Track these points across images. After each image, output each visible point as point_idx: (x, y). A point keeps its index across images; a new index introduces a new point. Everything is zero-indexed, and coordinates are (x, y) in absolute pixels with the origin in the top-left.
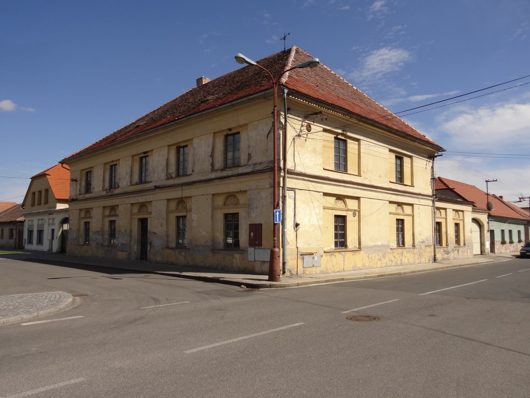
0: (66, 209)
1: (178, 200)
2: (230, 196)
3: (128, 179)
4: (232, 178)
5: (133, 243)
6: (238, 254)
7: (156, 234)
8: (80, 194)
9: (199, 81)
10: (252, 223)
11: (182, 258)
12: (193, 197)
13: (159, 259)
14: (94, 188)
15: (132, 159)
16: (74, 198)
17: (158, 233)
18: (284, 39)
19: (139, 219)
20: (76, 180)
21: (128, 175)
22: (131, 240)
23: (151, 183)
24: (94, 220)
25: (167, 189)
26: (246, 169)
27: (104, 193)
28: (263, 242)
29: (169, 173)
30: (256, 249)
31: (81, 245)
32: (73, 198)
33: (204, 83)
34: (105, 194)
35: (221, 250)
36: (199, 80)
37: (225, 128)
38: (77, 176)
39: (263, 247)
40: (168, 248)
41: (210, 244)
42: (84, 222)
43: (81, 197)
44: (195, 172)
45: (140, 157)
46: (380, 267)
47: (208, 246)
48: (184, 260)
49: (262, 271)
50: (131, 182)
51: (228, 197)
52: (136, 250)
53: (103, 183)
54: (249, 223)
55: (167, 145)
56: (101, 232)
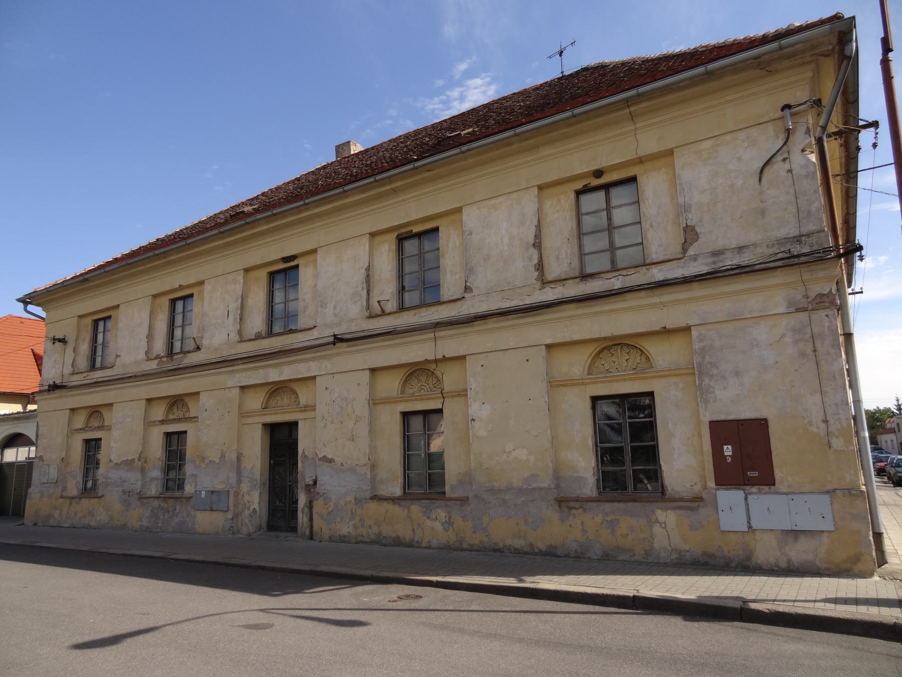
0: (18, 413)
2: (608, 348)
3: (231, 325)
4: (628, 296)
5: (245, 487)
6: (669, 512)
7: (331, 461)
8: (73, 374)
9: (343, 149)
10: (716, 418)
11: (438, 526)
12: (472, 357)
13: (345, 528)
14: (119, 356)
15: (245, 278)
16: (58, 382)
17: (338, 460)
18: (560, 55)
19: (265, 425)
20: (64, 339)
21: (231, 318)
22: (239, 481)
23: (312, 331)
24: (116, 433)
25: (377, 342)
26: (682, 267)
27: (153, 365)
28: (778, 474)
29: (379, 302)
30: (750, 493)
31: (73, 498)
32: (54, 382)
33: (352, 153)
34: (155, 367)
35: (590, 500)
36: (340, 148)
37: (586, 170)
38: (67, 329)
39: (780, 486)
40: (376, 498)
41: (546, 482)
42: (84, 440)
43: (77, 380)
44: (475, 292)
45: (268, 272)
46: (368, 495)
47: (541, 489)
48: (446, 530)
49: (789, 561)
50: (240, 332)
51: (92, 414)
52: (256, 506)
53: (148, 342)
54: (706, 417)
55: (369, 231)
56: (140, 463)
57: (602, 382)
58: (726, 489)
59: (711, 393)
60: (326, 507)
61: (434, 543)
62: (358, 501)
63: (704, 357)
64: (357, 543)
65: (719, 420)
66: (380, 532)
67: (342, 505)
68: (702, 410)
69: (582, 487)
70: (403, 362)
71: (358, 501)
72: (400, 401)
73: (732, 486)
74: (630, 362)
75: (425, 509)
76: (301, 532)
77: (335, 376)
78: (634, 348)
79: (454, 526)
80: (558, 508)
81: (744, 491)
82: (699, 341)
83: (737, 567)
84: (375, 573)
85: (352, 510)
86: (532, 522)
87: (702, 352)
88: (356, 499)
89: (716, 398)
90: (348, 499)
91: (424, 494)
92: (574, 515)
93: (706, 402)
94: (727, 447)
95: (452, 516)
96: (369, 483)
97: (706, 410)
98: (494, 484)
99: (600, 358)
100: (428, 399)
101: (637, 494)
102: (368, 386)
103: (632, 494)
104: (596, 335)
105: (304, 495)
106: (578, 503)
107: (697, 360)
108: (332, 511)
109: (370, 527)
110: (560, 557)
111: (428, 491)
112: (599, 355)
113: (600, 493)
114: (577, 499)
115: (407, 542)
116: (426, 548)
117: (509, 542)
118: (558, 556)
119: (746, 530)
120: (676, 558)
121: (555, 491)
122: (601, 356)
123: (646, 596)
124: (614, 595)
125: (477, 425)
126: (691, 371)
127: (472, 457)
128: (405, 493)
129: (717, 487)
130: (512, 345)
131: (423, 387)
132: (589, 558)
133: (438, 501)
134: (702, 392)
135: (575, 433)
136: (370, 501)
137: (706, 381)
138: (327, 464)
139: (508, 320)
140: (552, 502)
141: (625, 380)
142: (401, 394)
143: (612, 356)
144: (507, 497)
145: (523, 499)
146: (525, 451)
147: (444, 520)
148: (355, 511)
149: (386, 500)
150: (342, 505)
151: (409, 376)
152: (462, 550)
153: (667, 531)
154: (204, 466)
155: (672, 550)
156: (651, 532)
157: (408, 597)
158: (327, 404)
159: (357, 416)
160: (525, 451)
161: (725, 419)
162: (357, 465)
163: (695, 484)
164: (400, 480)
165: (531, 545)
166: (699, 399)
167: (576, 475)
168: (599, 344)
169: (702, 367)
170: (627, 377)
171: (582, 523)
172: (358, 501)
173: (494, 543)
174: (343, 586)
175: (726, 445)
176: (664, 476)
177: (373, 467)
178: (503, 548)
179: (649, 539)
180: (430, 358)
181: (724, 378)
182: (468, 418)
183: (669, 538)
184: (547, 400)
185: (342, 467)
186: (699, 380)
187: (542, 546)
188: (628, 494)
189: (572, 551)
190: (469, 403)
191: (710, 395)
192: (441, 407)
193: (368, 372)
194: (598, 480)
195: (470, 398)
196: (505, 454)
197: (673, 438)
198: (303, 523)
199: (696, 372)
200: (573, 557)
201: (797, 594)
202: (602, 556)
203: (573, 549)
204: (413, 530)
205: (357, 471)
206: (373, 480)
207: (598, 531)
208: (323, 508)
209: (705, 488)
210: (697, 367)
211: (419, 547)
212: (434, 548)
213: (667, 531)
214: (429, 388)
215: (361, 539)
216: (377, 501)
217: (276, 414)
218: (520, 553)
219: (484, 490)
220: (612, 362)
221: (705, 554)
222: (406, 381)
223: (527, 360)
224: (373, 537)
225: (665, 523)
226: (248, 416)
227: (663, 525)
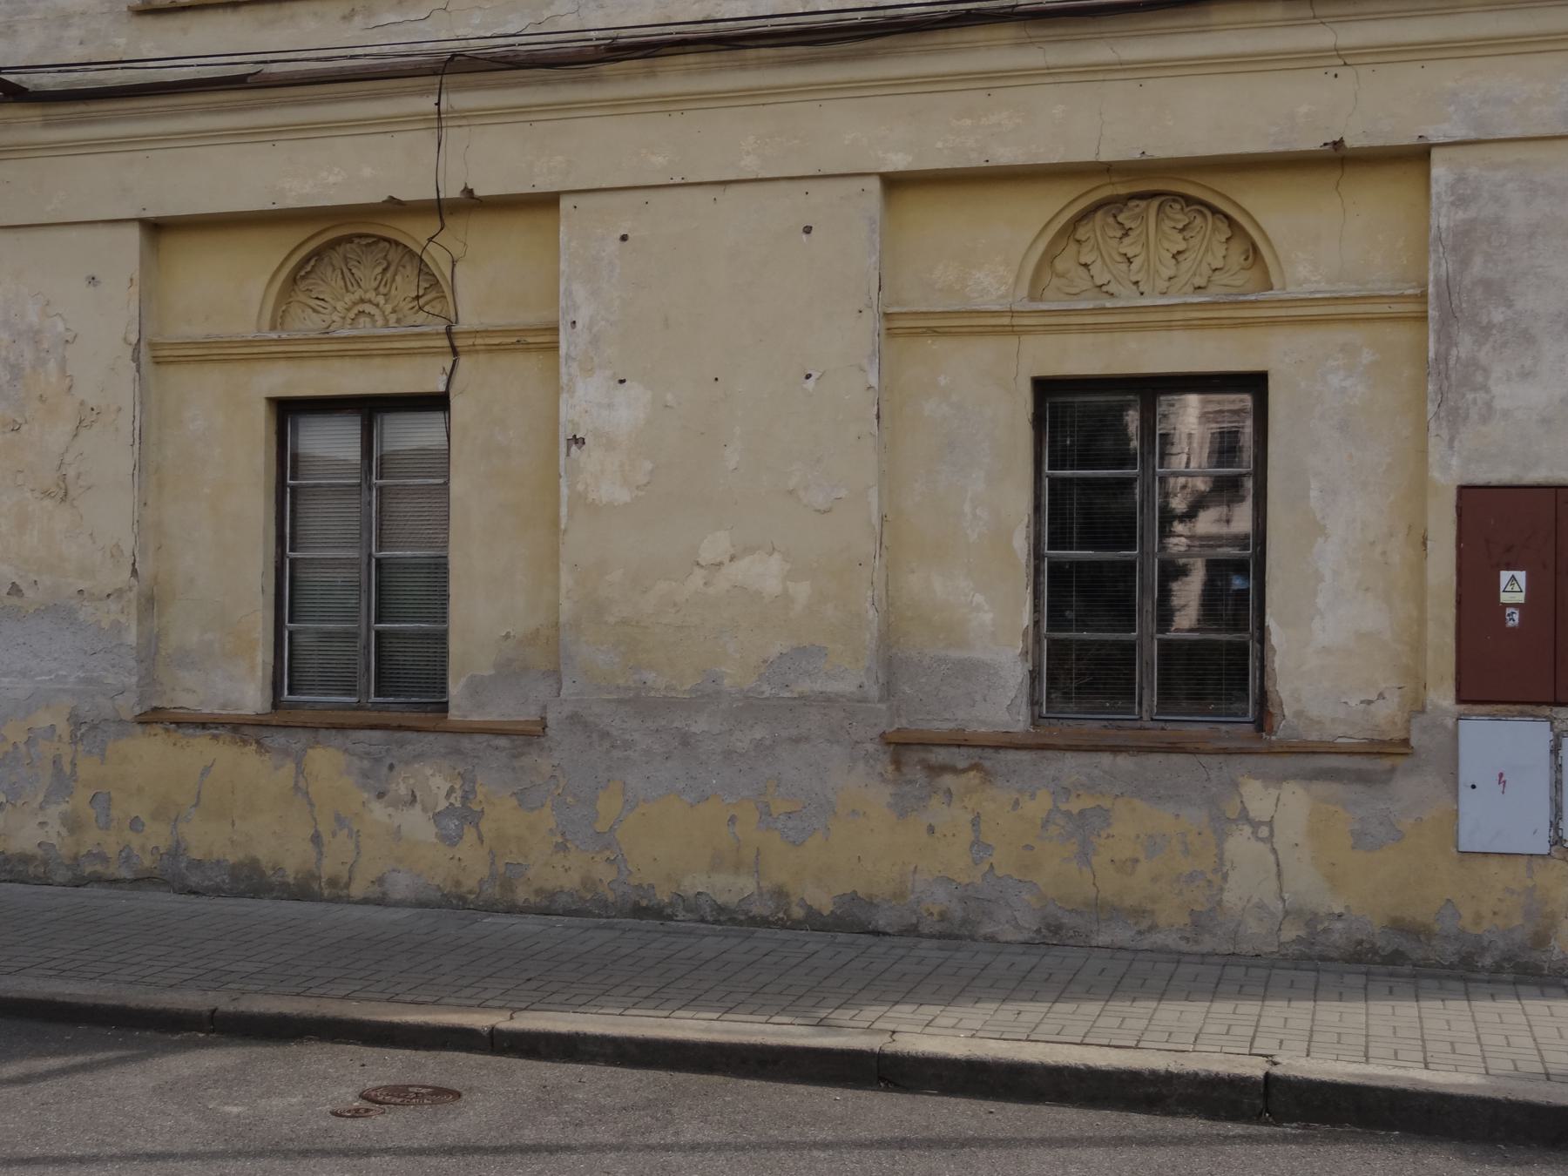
1: (309, 230)
10: (1483, 474)
11: (417, 824)
35: (1005, 744)
46: (129, 706)
47: (829, 700)
48: (451, 840)
57: (1083, 328)
58: (1494, 717)
59: (1474, 390)
61: (401, 886)
63: (1465, 263)
64: (79, 882)
65: (1494, 483)
66: (178, 841)
68: (1436, 448)
69: (978, 697)
70: (291, 202)
71: (84, 729)
72: (271, 357)
73: (1512, 708)
74: (1187, 264)
75: (366, 764)
78: (1209, 214)
79: (485, 826)
80: (890, 768)
81: (1552, 723)
82: (1453, 203)
83: (1498, 968)
84: (224, 1003)
85: (56, 762)
86: (789, 815)
87: (1463, 241)
88: (76, 721)
89: (1489, 405)
90: (43, 720)
91: (358, 707)
92: (949, 792)
93: (1456, 418)
94: (1513, 576)
95: (479, 789)
96: (132, 663)
97: (1451, 447)
98: (650, 677)
99: (1078, 241)
100: (389, 354)
101: (1169, 726)
102: (135, 289)
103: (1150, 724)
104: (1083, 154)
106: (963, 750)
107: (1438, 267)
109: (136, 824)
110: (885, 934)
111: (373, 699)
112: (1075, 229)
113: (1036, 719)
114: (959, 742)
115: (291, 880)
116: (365, 901)
117: (696, 883)
118: (877, 933)
119: (1544, 848)
120: (1299, 940)
121: (883, 706)
122: (1082, 233)
123: (1313, 1077)
124: (1196, 1074)
125: (590, 459)
126: (1411, 307)
127: (566, 579)
128: (276, 704)
129: (1462, 708)
130: (750, 166)
131: (368, 308)
132: (990, 939)
133: (422, 735)
134: (1446, 383)
135: (967, 508)
136: (139, 728)
137: (1465, 345)
139: (743, 67)
140: (870, 747)
141: (1168, 326)
142: (273, 328)
143: (1126, 234)
144: (700, 725)
145: (758, 736)
146: (775, 564)
147: (443, 805)
148: (74, 764)
149: (204, 725)
151: (307, 260)
152: (511, 909)
153: (1274, 851)
155: (1287, 913)
156: (1220, 857)
157: (400, 1095)
159: (82, 403)
160: (775, 564)
161: (1516, 482)
163: (1381, 696)
164: (263, 656)
165: (780, 894)
166: (1431, 408)
167: (955, 654)
168: (1090, 186)
169: (1454, 298)
170: (1178, 315)
171: (976, 822)
172: (84, 728)
173: (640, 886)
174: (100, 1056)
175: (1508, 568)
176: (1277, 665)
177: (150, 603)
178: (671, 904)
179: (1210, 876)
180: (409, 193)
181: (1527, 338)
182: (557, 430)
183: (1279, 875)
184: (874, 381)
185: (15, 600)
186: (1438, 341)
187: (824, 902)
188: (1138, 724)
189: (932, 914)
190: (564, 379)
191: (1470, 396)
192: (442, 388)
193: (134, 234)
194: (1034, 675)
195: (568, 356)
196: (697, 570)
197: (1320, 540)
199: (1433, 313)
200: (931, 936)
201: (1256, 1031)
202: (1038, 931)
203: (936, 910)
204: (316, 839)
205: (81, 616)
206: (150, 654)
207: (1029, 847)
209: (1418, 708)
210: (1438, 296)
211: (336, 900)
212: (398, 904)
213: (1274, 851)
214: (394, 311)
215: (99, 868)
216: (167, 730)
218: (733, 921)
219: (609, 701)
220: (1119, 259)
221: (1399, 926)
222: (295, 281)
223: (808, 230)
224: (148, 862)
225: (1270, 824)
227: (1264, 832)
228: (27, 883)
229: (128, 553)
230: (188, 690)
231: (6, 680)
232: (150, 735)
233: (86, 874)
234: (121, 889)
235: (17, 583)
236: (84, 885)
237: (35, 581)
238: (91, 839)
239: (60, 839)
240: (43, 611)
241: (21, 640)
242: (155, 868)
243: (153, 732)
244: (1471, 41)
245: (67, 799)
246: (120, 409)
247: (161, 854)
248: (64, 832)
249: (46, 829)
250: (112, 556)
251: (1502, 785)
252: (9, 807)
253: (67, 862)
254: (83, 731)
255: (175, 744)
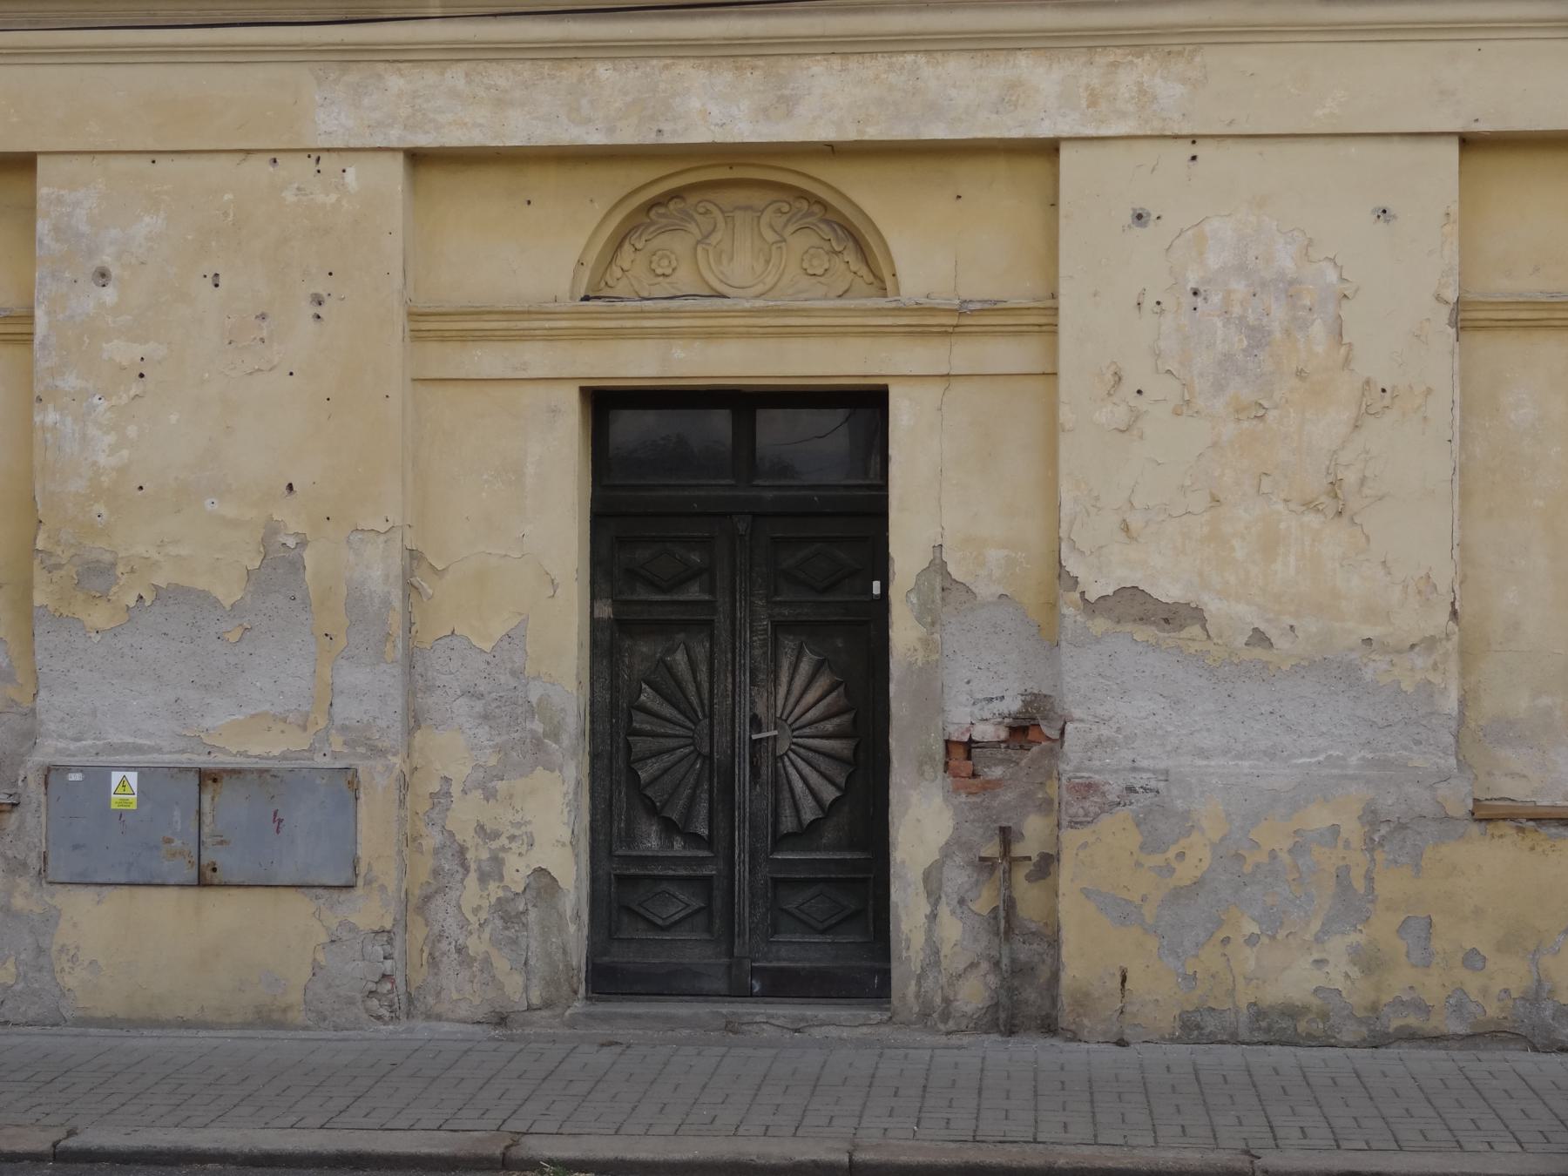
7: (1173, 617)
60: (1157, 860)
62: (1384, 830)
64: (1378, 1041)
66: (1539, 981)
67: (1273, 855)
76: (917, 996)
77: (1201, 149)
85: (1342, 876)
88: (1371, 818)
90: (1318, 818)
105: (938, 800)
108: (1199, 883)
109: (1473, 959)
136: (1475, 829)
138: (1144, 633)
148: (1369, 878)
150: (1273, 855)
154: (98, 617)
158: (1149, 303)
162: (1368, 641)
172: (1384, 830)
185: (1259, 653)
198: (933, 949)
205: (1368, 675)
208: (1138, 864)
215: (1413, 1021)
216: (1521, 830)
217: (709, 335)
224: (1493, 1010)
226: (464, 337)
228: (1296, 1045)
229: (1443, 587)
230: (1513, 775)
231: (1246, 764)
232: (1493, 836)
233: (1391, 1030)
234: (1446, 1048)
235: (1262, 628)
236: (1387, 1046)
237: (1292, 627)
238: (1399, 981)
239: (1349, 982)
240: (1304, 667)
241: (1265, 709)
242: (1505, 1018)
243: (1497, 833)
244: (1053, 31)
245: (1359, 927)
246: (1429, 391)
247: (1514, 999)
248: (1355, 972)
249: (1327, 969)
250: (1420, 592)
251: (277, 823)
252: (1265, 940)
253: (1360, 1014)
254: (1383, 832)
255: (1532, 849)
